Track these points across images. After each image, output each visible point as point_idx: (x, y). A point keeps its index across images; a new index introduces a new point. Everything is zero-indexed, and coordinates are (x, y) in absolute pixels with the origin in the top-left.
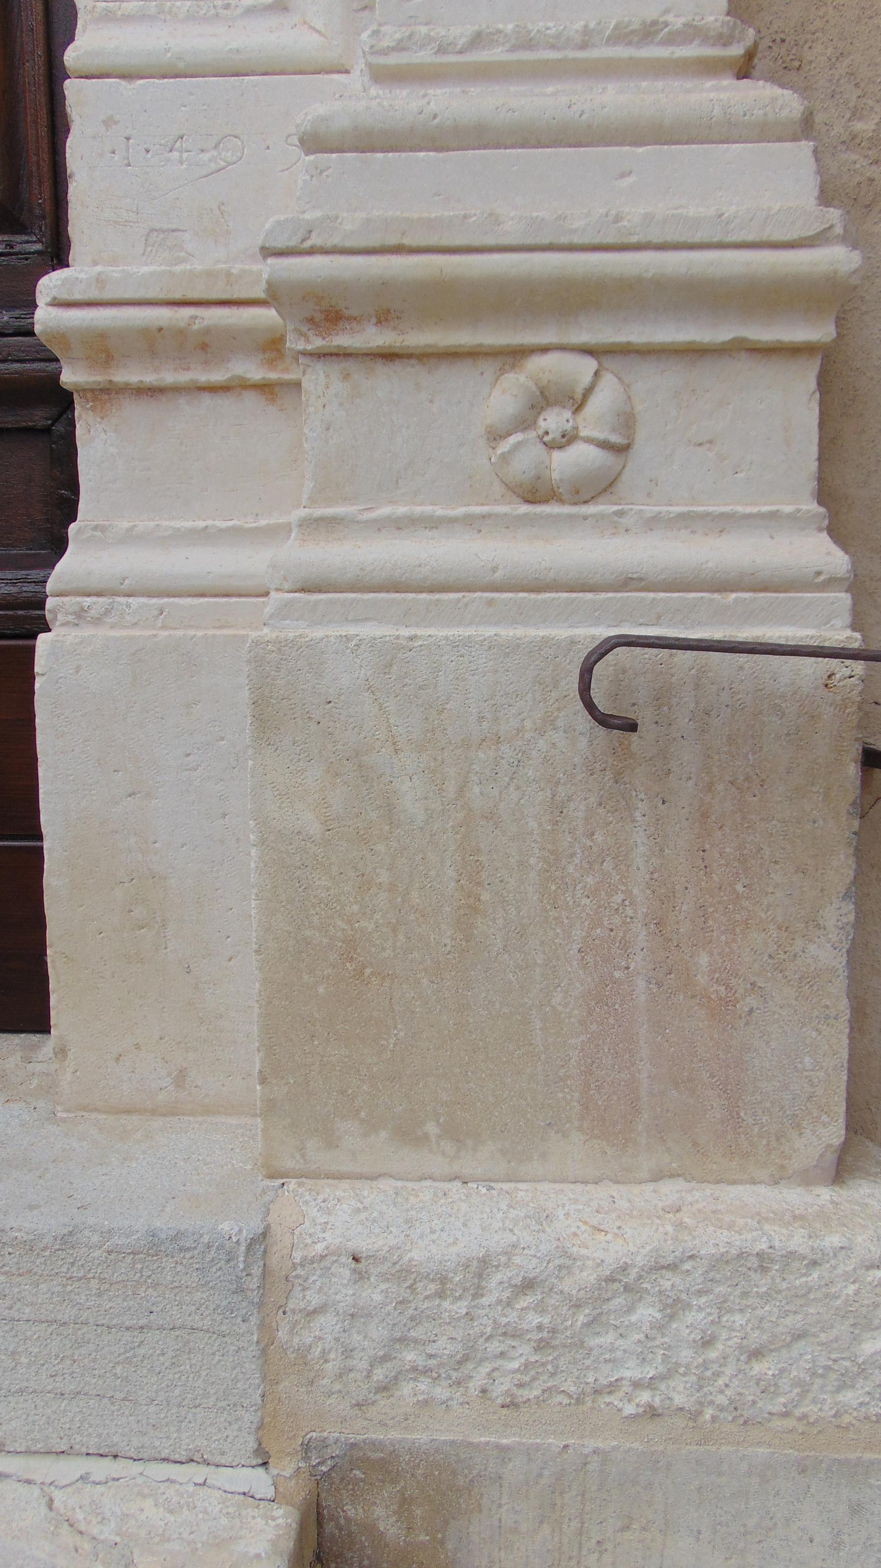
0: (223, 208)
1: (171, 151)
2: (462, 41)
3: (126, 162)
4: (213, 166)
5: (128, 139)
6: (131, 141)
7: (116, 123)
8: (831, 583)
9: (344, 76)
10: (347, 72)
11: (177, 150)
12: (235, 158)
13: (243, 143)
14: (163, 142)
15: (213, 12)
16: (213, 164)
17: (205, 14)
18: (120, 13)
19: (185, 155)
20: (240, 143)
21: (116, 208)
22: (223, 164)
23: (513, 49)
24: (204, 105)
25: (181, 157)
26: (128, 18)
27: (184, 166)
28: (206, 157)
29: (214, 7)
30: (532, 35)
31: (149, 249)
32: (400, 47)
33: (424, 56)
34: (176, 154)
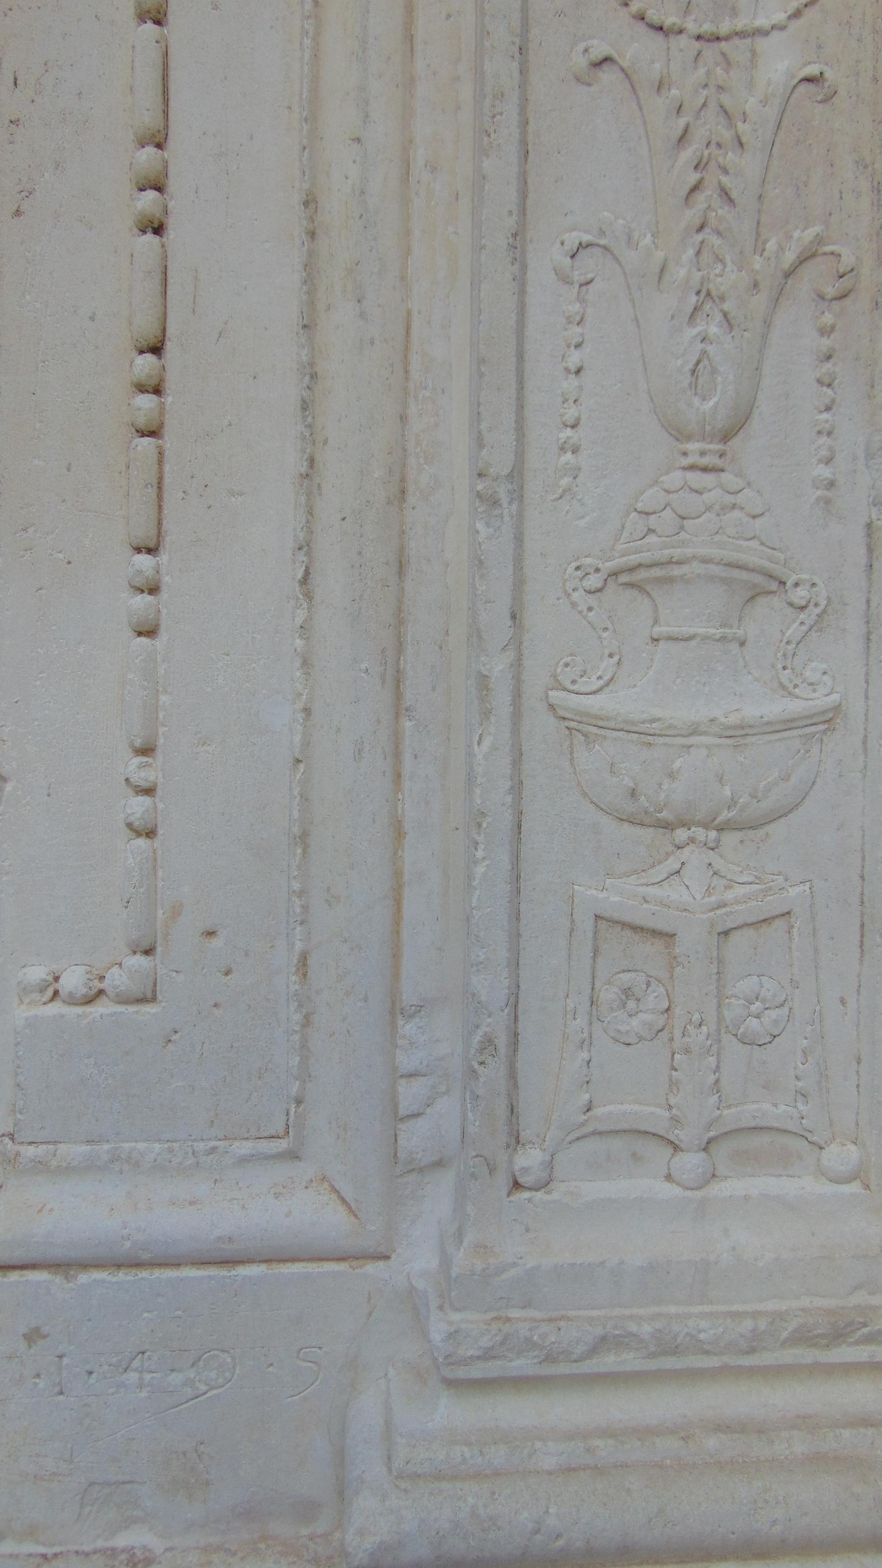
0: (202, 1448)
1: (126, 1370)
2: (580, 1349)
3: (57, 1389)
4: (189, 1391)
5: (60, 1357)
6: (65, 1361)
7: (45, 1337)
8: (865, 1422)
9: (381, 1264)
10: (387, 1258)
11: (136, 1370)
12: (221, 1380)
13: (233, 1358)
14: (114, 1360)
15: (191, 1161)
16: (189, 1390)
17: (180, 1163)
18: (54, 1163)
19: (148, 1376)
20: (229, 1360)
21: (38, 1455)
22: (203, 1388)
23: (653, 1355)
24: (179, 1309)
25: (141, 1379)
26: (68, 1170)
27: (144, 1394)
28: (176, 1378)
29: (193, 1153)
30: (679, 1340)
31: (87, 1510)
32: (487, 1355)
33: (522, 1365)
34: (133, 1376)
